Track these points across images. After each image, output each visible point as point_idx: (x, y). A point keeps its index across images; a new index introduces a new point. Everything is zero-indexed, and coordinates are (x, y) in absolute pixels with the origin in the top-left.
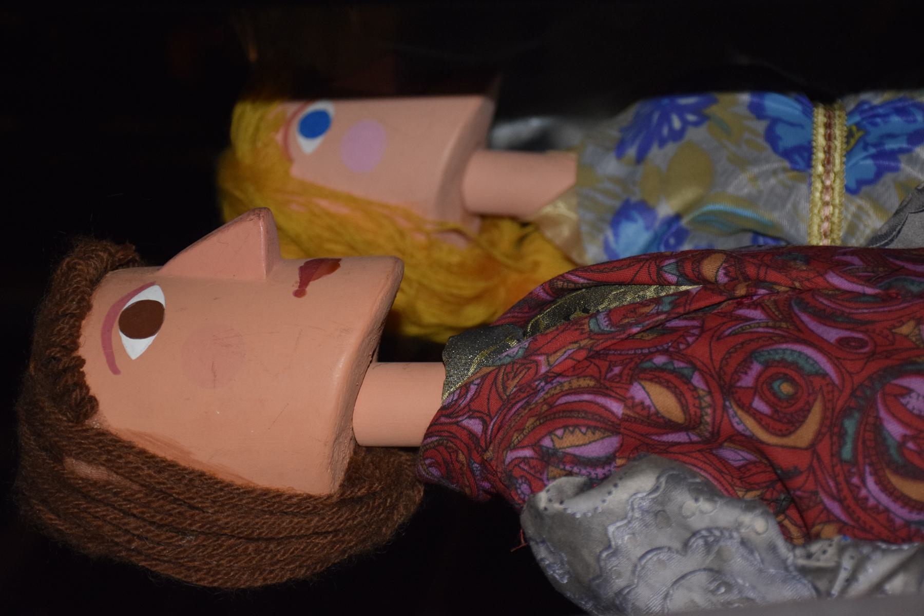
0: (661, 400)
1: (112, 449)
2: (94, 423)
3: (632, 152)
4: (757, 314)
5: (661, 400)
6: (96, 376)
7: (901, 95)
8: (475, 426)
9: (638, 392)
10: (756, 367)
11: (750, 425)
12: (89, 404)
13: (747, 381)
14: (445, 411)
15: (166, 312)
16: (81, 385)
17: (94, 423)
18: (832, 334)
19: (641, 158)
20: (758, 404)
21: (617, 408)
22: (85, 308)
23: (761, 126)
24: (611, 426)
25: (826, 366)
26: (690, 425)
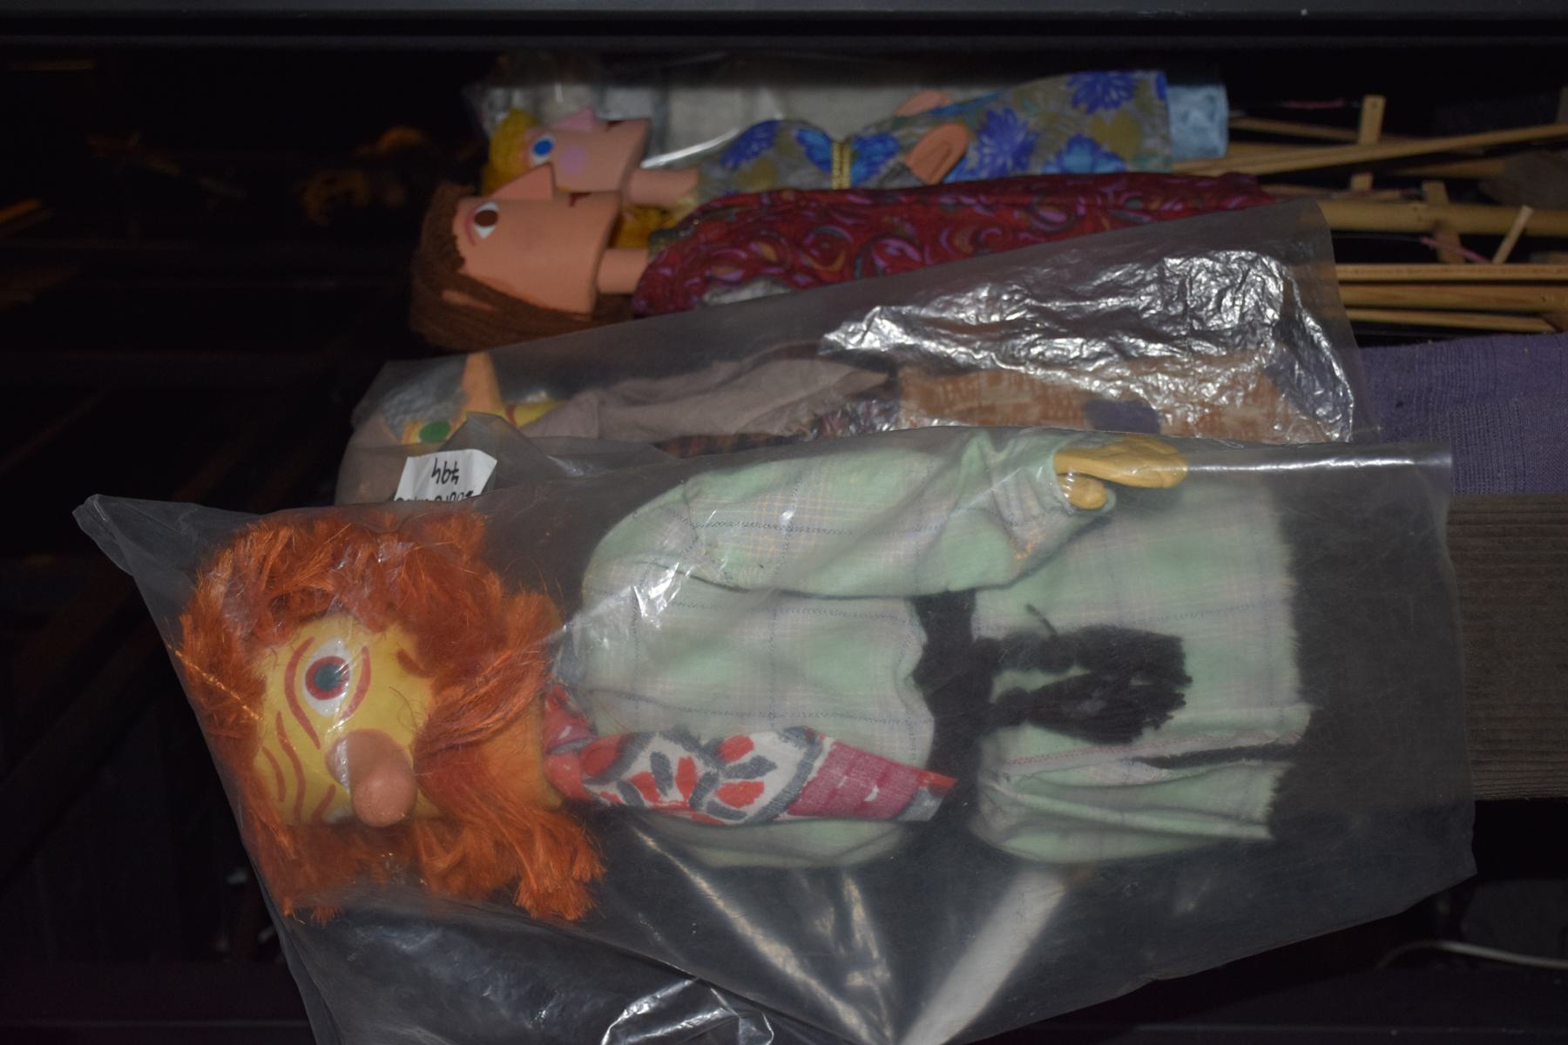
0: (767, 251)
1: (475, 287)
2: (462, 271)
3: (730, 164)
4: (811, 214)
5: (767, 251)
6: (463, 246)
7: (977, 93)
8: (667, 272)
9: (754, 246)
10: (812, 236)
11: (807, 261)
12: (461, 261)
13: (807, 241)
14: (651, 267)
15: (137, 579)
16: (455, 251)
17: (462, 271)
18: (849, 222)
19: (735, 167)
20: (815, 253)
21: (743, 255)
22: (453, 239)
23: (803, 149)
24: (739, 264)
25: (845, 234)
26: (779, 264)
